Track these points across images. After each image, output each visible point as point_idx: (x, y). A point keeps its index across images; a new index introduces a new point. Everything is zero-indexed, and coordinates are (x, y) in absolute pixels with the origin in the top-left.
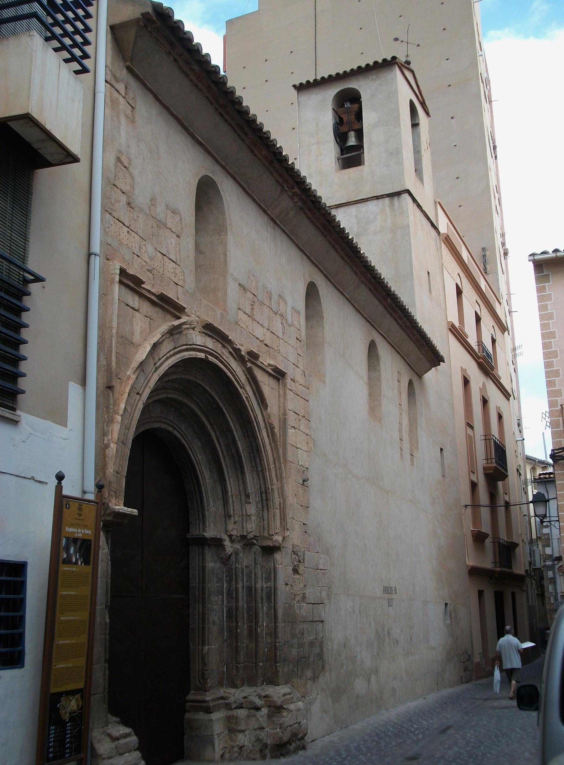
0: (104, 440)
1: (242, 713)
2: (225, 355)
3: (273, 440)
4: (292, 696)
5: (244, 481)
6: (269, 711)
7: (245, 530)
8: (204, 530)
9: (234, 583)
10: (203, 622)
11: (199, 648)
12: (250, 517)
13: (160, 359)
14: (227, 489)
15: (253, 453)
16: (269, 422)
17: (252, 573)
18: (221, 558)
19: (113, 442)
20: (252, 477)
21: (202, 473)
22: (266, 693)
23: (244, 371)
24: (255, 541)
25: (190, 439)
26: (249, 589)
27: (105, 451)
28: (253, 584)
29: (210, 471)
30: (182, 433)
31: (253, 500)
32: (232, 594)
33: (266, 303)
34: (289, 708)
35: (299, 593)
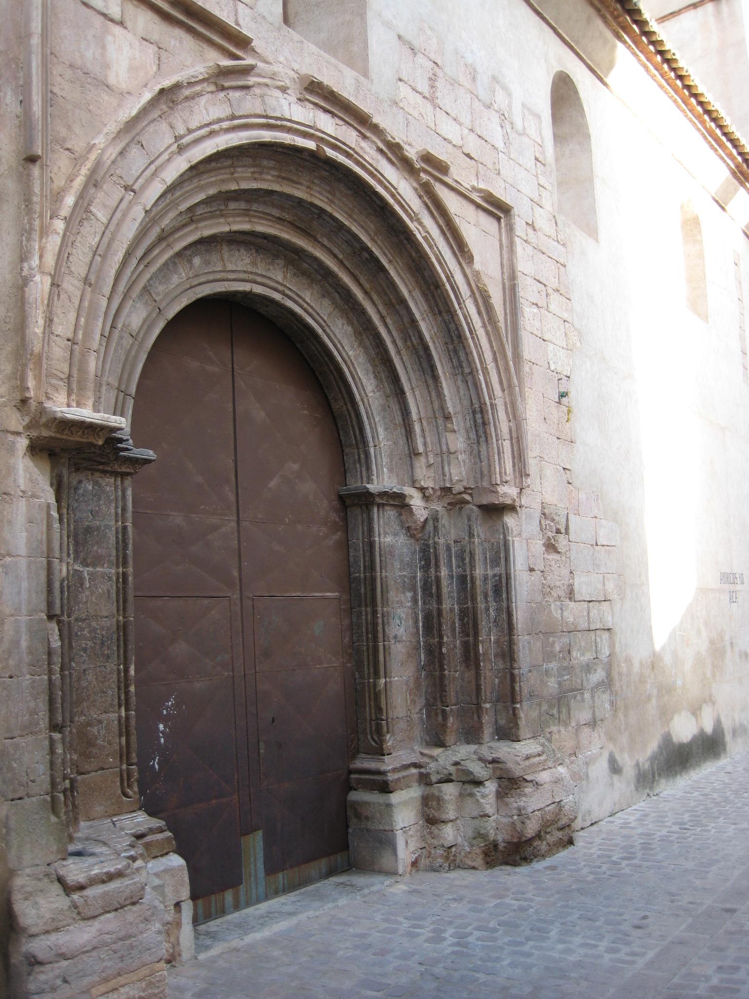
0: (22, 269)
1: (450, 791)
2: (368, 154)
3: (490, 319)
4: (542, 758)
5: (439, 391)
6: (500, 786)
7: (447, 477)
8: (369, 481)
9: (432, 570)
10: (375, 638)
11: (369, 682)
12: (455, 456)
13: (190, 131)
14: (409, 407)
15: (452, 343)
16: (478, 288)
17: (465, 551)
18: (408, 528)
19: (43, 273)
20: (456, 385)
21: (358, 380)
22: (494, 756)
23: (415, 189)
24: (467, 497)
25: (326, 319)
26: (462, 579)
27: (23, 292)
28: (468, 570)
29: (376, 377)
30: (305, 305)
31: (458, 425)
32: (431, 589)
33: (465, 84)
34: (537, 780)
35: (558, 583)
